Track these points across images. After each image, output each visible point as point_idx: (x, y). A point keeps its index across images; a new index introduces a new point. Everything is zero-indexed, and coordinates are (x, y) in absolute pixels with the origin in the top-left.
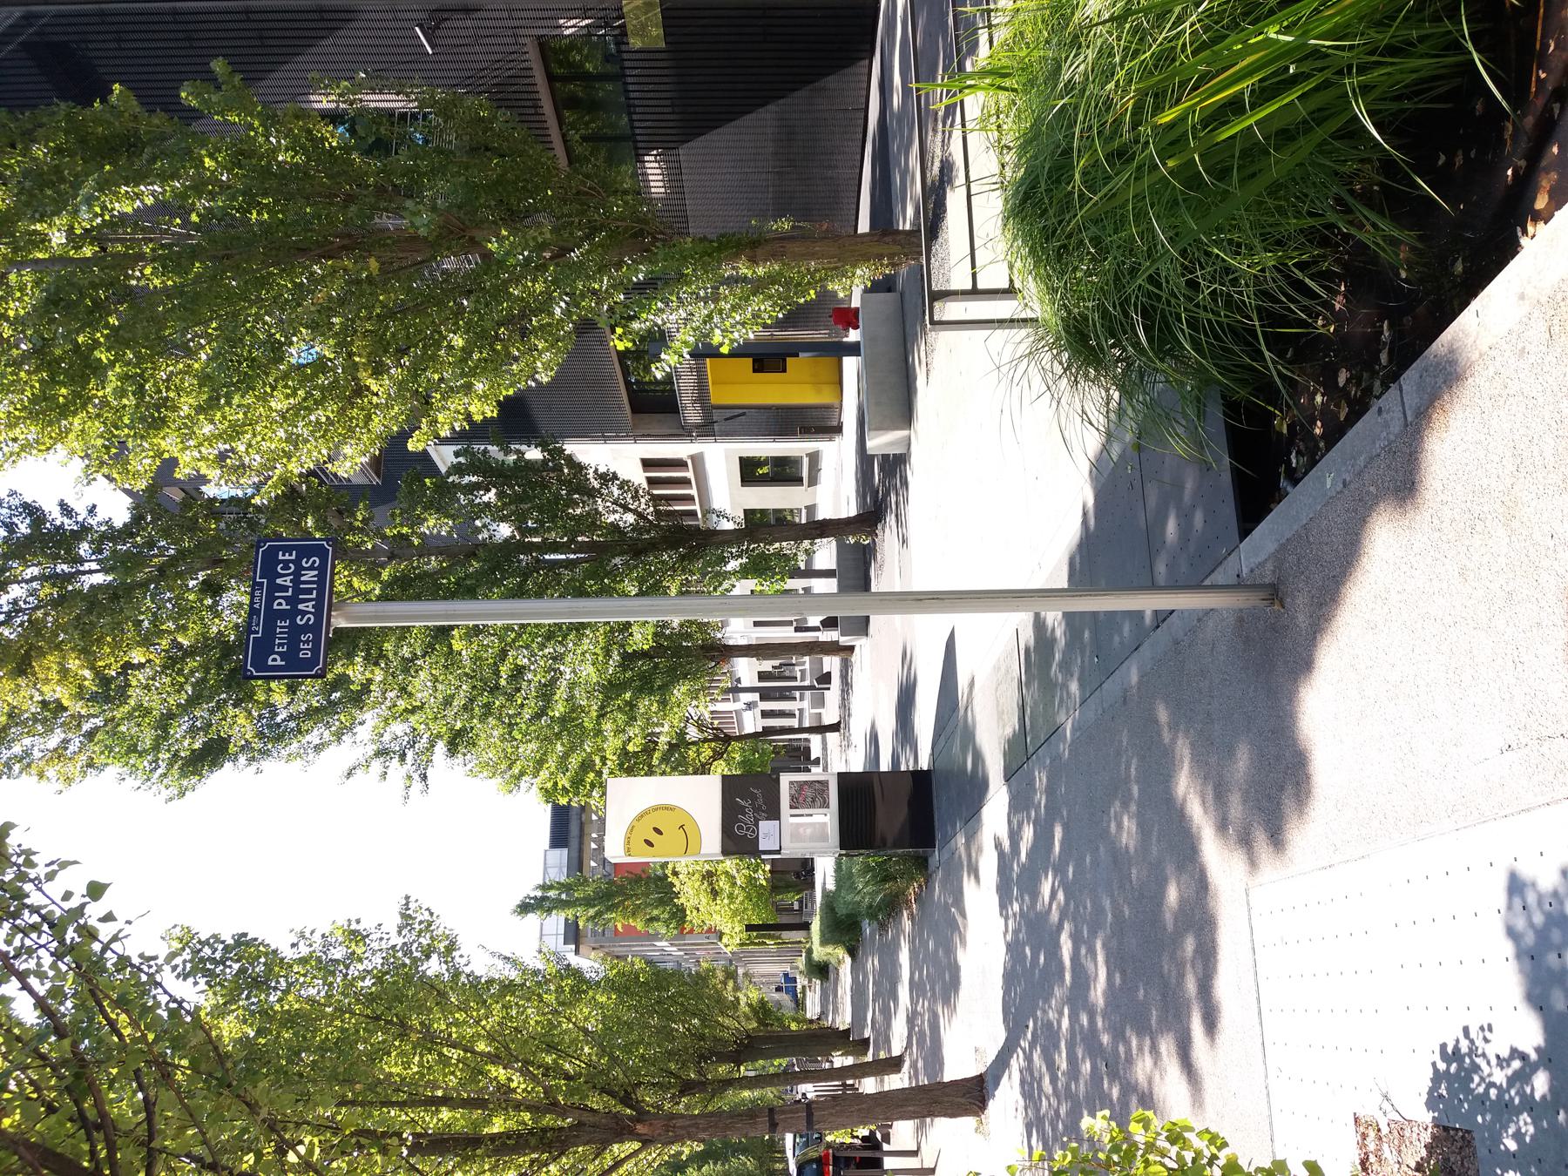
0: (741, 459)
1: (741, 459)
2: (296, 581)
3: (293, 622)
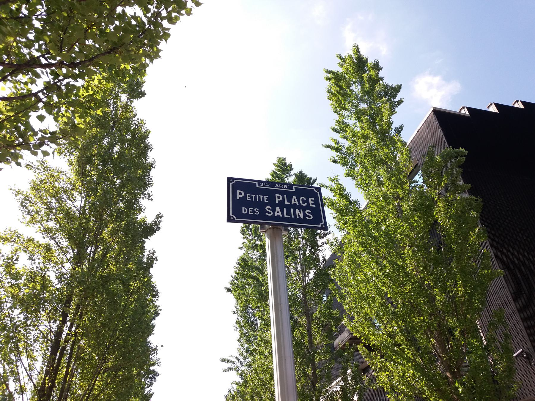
0: (229, 180)
1: (229, 180)
2: (295, 207)
3: (267, 204)
